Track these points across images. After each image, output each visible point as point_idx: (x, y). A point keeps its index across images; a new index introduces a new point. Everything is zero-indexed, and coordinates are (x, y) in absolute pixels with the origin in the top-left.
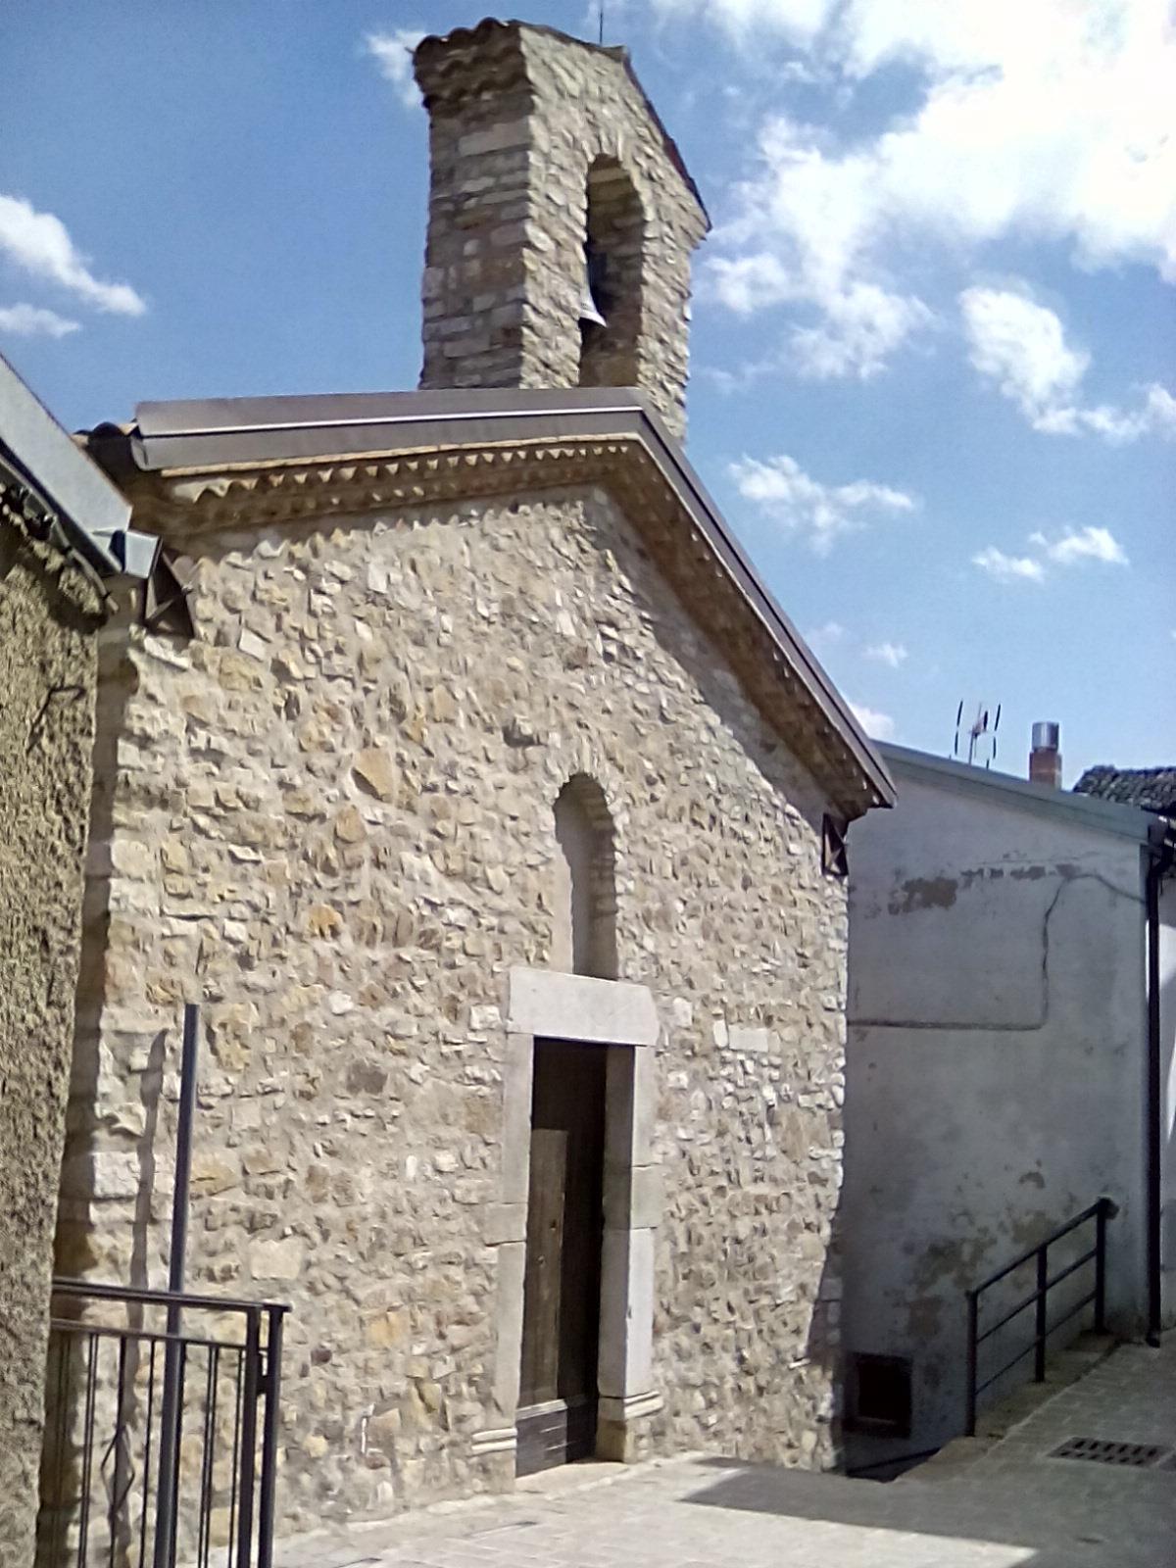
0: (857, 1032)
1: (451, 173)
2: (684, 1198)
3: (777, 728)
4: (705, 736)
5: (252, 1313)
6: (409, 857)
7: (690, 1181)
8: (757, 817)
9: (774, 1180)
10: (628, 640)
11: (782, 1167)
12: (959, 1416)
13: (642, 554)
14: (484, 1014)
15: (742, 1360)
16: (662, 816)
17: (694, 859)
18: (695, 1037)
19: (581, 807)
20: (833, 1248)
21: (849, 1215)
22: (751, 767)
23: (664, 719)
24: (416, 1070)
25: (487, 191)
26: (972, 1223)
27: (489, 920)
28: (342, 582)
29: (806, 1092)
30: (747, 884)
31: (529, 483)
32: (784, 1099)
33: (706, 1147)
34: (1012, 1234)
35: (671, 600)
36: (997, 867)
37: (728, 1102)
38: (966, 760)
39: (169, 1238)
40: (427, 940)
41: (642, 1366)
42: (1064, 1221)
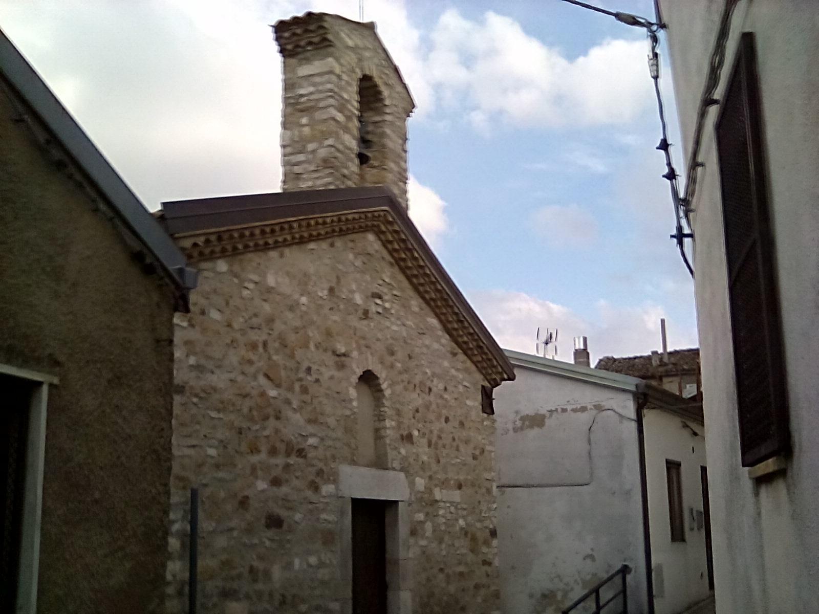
0: (500, 491)
3: (457, 343)
6: (290, 414)
10: (387, 305)
13: (391, 264)
24: (298, 517)
25: (311, 93)
26: (561, 581)
28: (256, 283)
30: (447, 420)
31: (339, 232)
34: (581, 585)
36: (565, 407)
38: (542, 356)
39: (187, 602)
40: (301, 453)
42: (605, 576)
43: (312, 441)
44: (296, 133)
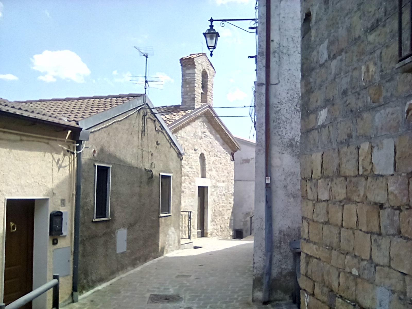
1: (185, 75)
2: (214, 205)
4: (216, 144)
5: (189, 212)
7: (214, 203)
8: (222, 154)
9: (225, 203)
11: (225, 201)
12: (249, 233)
14: (193, 184)
15: (221, 227)
16: (211, 156)
17: (215, 161)
18: (215, 185)
19: (202, 157)
20: (232, 212)
21: (234, 208)
22: (221, 147)
23: (211, 143)
27: (193, 173)
29: (229, 191)
30: (221, 164)
32: (226, 192)
33: (216, 199)
35: (211, 127)
37: (219, 193)
40: (188, 176)
41: (210, 226)
43: (190, 172)
44: (185, 89)
